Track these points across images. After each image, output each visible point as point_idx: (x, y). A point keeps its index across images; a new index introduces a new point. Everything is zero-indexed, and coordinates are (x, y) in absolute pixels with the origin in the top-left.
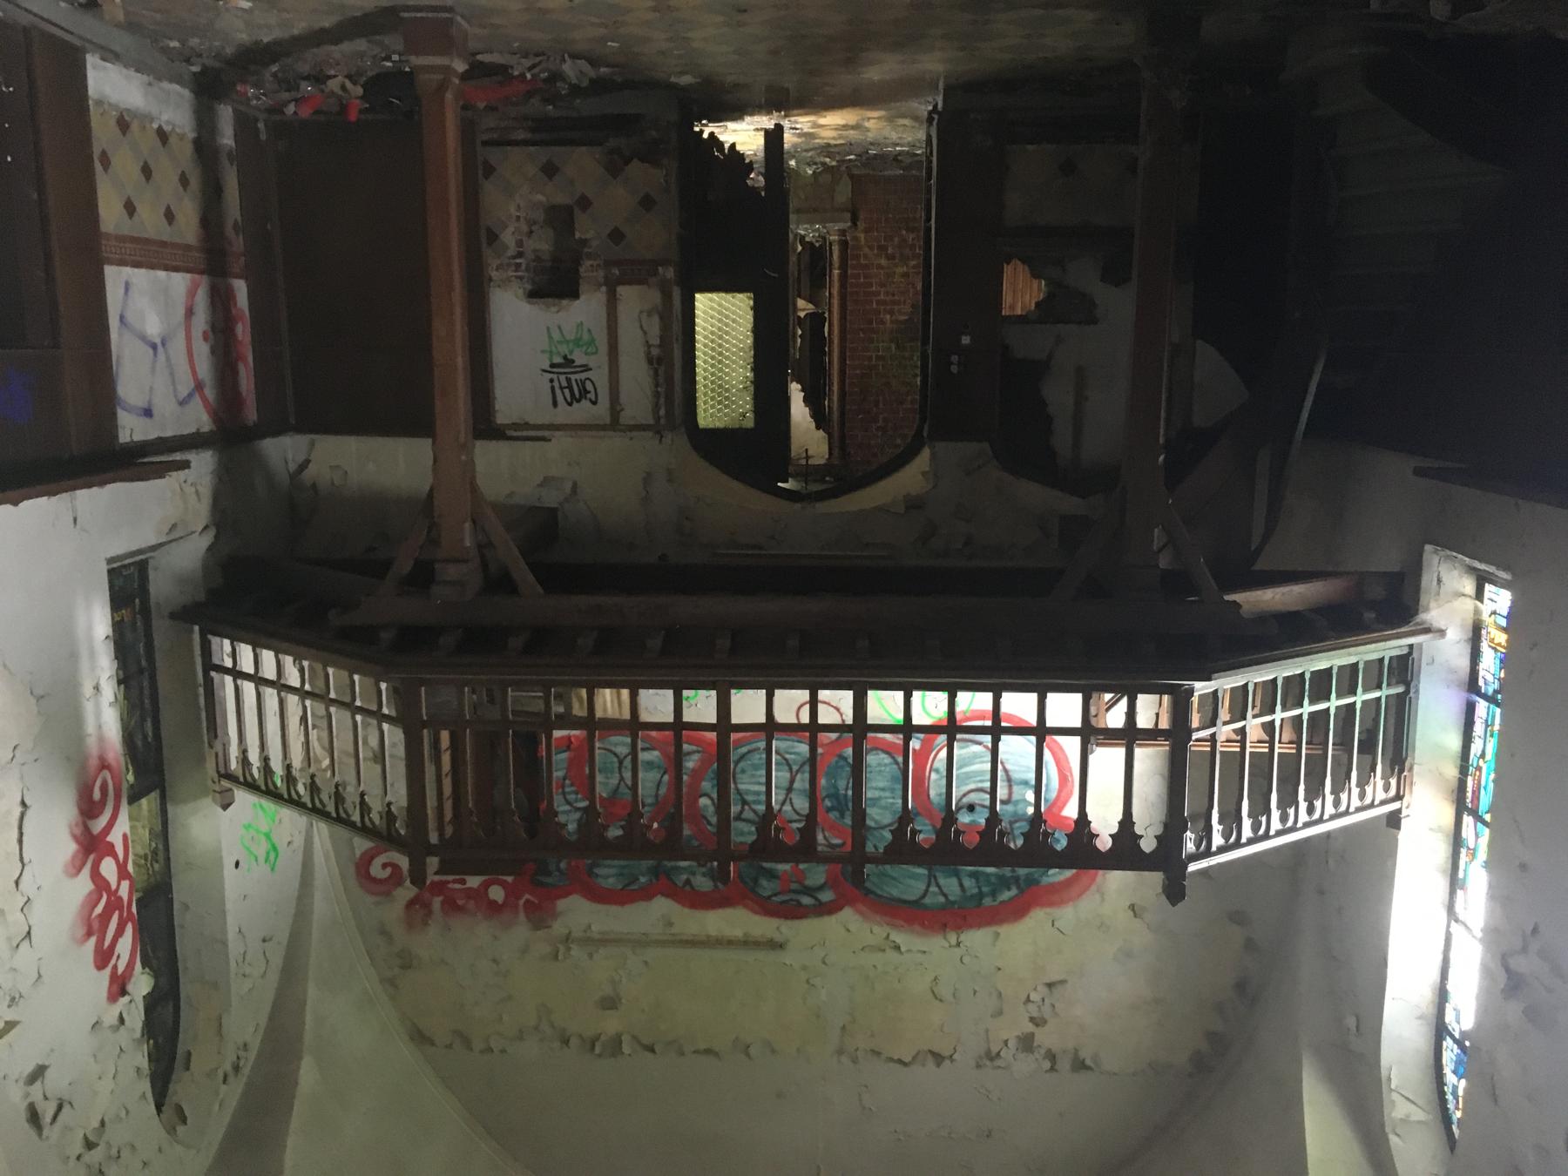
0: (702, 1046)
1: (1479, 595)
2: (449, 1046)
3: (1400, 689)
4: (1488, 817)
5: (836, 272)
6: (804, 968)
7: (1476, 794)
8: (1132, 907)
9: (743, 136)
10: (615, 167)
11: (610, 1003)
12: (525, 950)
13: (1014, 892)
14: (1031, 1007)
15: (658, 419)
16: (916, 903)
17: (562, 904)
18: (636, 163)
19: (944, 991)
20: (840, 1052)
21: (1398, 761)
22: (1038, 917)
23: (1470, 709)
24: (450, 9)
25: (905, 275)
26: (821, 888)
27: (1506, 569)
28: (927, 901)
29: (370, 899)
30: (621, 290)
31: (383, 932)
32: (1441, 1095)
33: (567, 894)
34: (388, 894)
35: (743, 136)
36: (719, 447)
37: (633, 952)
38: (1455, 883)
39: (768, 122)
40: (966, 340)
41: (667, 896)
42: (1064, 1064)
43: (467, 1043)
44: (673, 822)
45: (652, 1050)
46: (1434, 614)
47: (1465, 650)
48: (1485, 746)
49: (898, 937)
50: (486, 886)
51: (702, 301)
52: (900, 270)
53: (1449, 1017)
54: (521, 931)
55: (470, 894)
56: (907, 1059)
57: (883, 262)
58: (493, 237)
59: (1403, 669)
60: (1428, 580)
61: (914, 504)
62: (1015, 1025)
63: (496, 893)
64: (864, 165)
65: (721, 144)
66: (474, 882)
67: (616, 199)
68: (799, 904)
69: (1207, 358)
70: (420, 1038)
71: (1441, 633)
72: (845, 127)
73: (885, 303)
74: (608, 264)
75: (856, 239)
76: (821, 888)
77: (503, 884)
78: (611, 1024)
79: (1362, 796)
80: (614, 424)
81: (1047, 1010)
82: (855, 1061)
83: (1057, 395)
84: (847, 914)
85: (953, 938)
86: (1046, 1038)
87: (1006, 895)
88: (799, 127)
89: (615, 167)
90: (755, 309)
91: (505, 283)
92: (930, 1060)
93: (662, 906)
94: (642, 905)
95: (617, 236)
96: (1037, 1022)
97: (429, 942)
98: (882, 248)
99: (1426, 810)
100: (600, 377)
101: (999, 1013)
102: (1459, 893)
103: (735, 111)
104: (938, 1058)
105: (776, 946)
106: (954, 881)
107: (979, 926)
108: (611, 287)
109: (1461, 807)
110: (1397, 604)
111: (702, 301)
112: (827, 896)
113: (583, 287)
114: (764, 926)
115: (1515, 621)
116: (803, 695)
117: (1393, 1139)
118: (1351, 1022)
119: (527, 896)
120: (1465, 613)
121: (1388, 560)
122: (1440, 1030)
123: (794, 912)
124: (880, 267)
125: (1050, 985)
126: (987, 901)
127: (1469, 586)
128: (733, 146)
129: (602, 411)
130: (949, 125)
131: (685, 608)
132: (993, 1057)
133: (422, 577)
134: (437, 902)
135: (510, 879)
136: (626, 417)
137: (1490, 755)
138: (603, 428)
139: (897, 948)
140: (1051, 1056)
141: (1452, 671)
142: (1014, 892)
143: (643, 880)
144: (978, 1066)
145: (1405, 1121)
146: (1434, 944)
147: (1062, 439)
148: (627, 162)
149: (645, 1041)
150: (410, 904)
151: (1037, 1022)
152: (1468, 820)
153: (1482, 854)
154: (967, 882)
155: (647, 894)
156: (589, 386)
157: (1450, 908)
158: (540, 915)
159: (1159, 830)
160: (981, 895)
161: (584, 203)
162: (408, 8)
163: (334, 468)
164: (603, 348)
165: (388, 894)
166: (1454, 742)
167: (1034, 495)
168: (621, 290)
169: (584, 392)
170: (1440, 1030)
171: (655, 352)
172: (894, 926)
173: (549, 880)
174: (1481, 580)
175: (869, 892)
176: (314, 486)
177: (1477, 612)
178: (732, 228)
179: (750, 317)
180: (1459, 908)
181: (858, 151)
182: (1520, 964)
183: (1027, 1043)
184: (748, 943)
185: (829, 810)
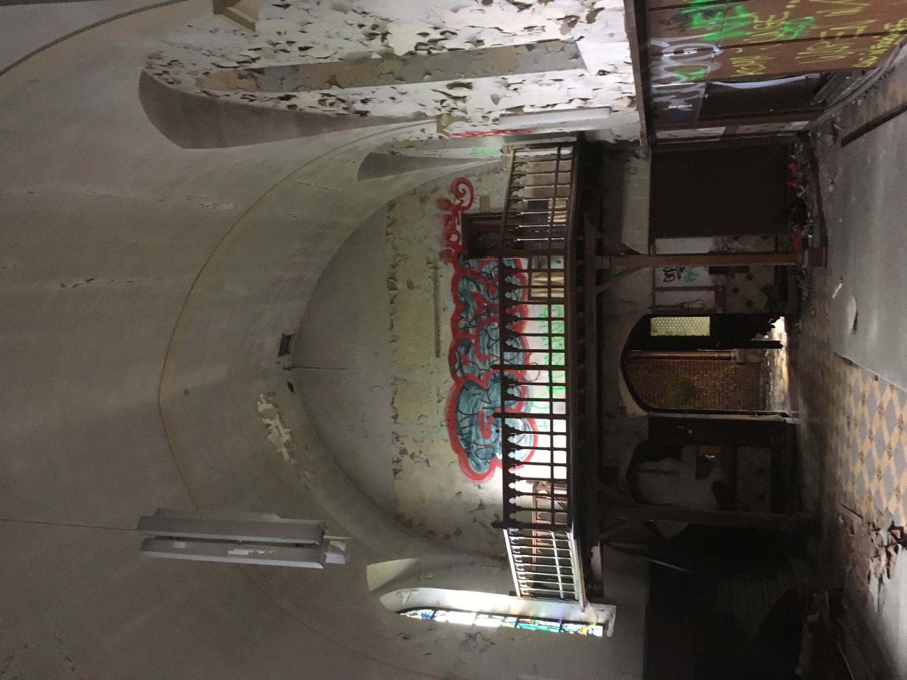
0: (395, 324)
1: (598, 624)
2: (388, 218)
3: (562, 596)
4: (518, 627)
5: (716, 355)
6: (429, 365)
7: (524, 622)
8: (460, 493)
9: (779, 329)
10: (765, 290)
11: (410, 285)
12: (430, 249)
13: (464, 447)
14: (418, 454)
15: (658, 306)
16: (457, 409)
17: (451, 265)
18: (767, 298)
19: (423, 420)
20: (396, 379)
21: (534, 596)
22: (455, 457)
23: (556, 621)
24: (826, 265)
25: (715, 386)
26: (462, 371)
27: (614, 634)
28: (459, 414)
29: (450, 184)
30: (712, 293)
31: (436, 190)
32: (410, 609)
33: (455, 267)
34: (452, 191)
35: (779, 329)
36: (644, 324)
37: (432, 296)
38: (491, 614)
39: (784, 341)
40: (690, 432)
41: (456, 309)
42: (396, 466)
43: (389, 226)
44: (511, 349)
45: (392, 302)
46: (590, 608)
47: (578, 619)
48: (544, 626)
49: (444, 401)
50: (458, 233)
51: (708, 319)
52: (717, 383)
53: (440, 612)
54: (439, 248)
55: (454, 226)
56: (394, 405)
57: (721, 376)
58: (736, 239)
59: (569, 598)
60: (602, 606)
61: (623, 410)
62: (411, 448)
63: (454, 238)
64: (765, 368)
65: (774, 321)
66: (459, 228)
67: (750, 293)
68: (455, 363)
69: (683, 525)
70: (392, 205)
71: (583, 611)
72: (781, 370)
73: (702, 376)
74: (724, 287)
75: (732, 364)
76: (462, 371)
77: (458, 241)
78: (401, 285)
79: (523, 584)
80: (656, 289)
81: (418, 459)
82: (392, 384)
83: (666, 464)
84: (452, 382)
85: (444, 423)
86: (406, 459)
87: (463, 444)
88: (782, 356)
89: (765, 290)
90: (703, 336)
91: (716, 243)
92: (394, 414)
93: (452, 307)
94: (452, 298)
95: (736, 290)
96: (412, 456)
97: (432, 208)
98: (727, 375)
99: (516, 605)
100: (676, 283)
101: (415, 441)
102: (487, 616)
103: (789, 329)
104: (395, 417)
105: (438, 354)
106: (467, 424)
107: (450, 434)
108: (714, 288)
109: (519, 617)
110: (594, 596)
111: (708, 319)
112: (459, 374)
113: (714, 276)
114: (445, 348)
115: (591, 637)
116: (563, 396)
117: (395, 593)
118: (430, 576)
119: (453, 251)
120: (592, 621)
121: (608, 592)
122: (435, 609)
123: (452, 360)
124: (719, 374)
125: (427, 461)
126: (460, 437)
127: (601, 620)
128: (774, 327)
129: (661, 283)
130: (780, 427)
131: (592, 349)
132: (397, 438)
133: (600, 250)
134: (450, 213)
135: (460, 243)
136: (658, 294)
137: (540, 627)
138: (654, 282)
139: (439, 402)
140: (398, 461)
141: (569, 615)
142: (464, 447)
143: (462, 299)
144: (393, 433)
145: (402, 597)
146: (468, 607)
147: (648, 465)
148: (767, 295)
149: (395, 300)
150: (448, 201)
151: (412, 456)
152: (515, 619)
153: (505, 625)
154: (467, 430)
155: (456, 300)
156: (672, 278)
157: (479, 613)
158: (446, 256)
159: (518, 520)
160: (462, 434)
161: (750, 277)
162: (827, 249)
163: (636, 168)
164: (690, 284)
165: (452, 191)
166: (542, 615)
167: (626, 459)
168: (712, 293)
169: (668, 276)
170: (435, 609)
171: (686, 305)
172: (448, 399)
173: (461, 260)
174: (605, 626)
175: (462, 391)
176: (629, 161)
177: (592, 623)
178: (739, 330)
179: (699, 334)
180: (481, 616)
181: (772, 369)
182: (479, 638)
183: (403, 452)
184: (438, 342)
185: (495, 375)
